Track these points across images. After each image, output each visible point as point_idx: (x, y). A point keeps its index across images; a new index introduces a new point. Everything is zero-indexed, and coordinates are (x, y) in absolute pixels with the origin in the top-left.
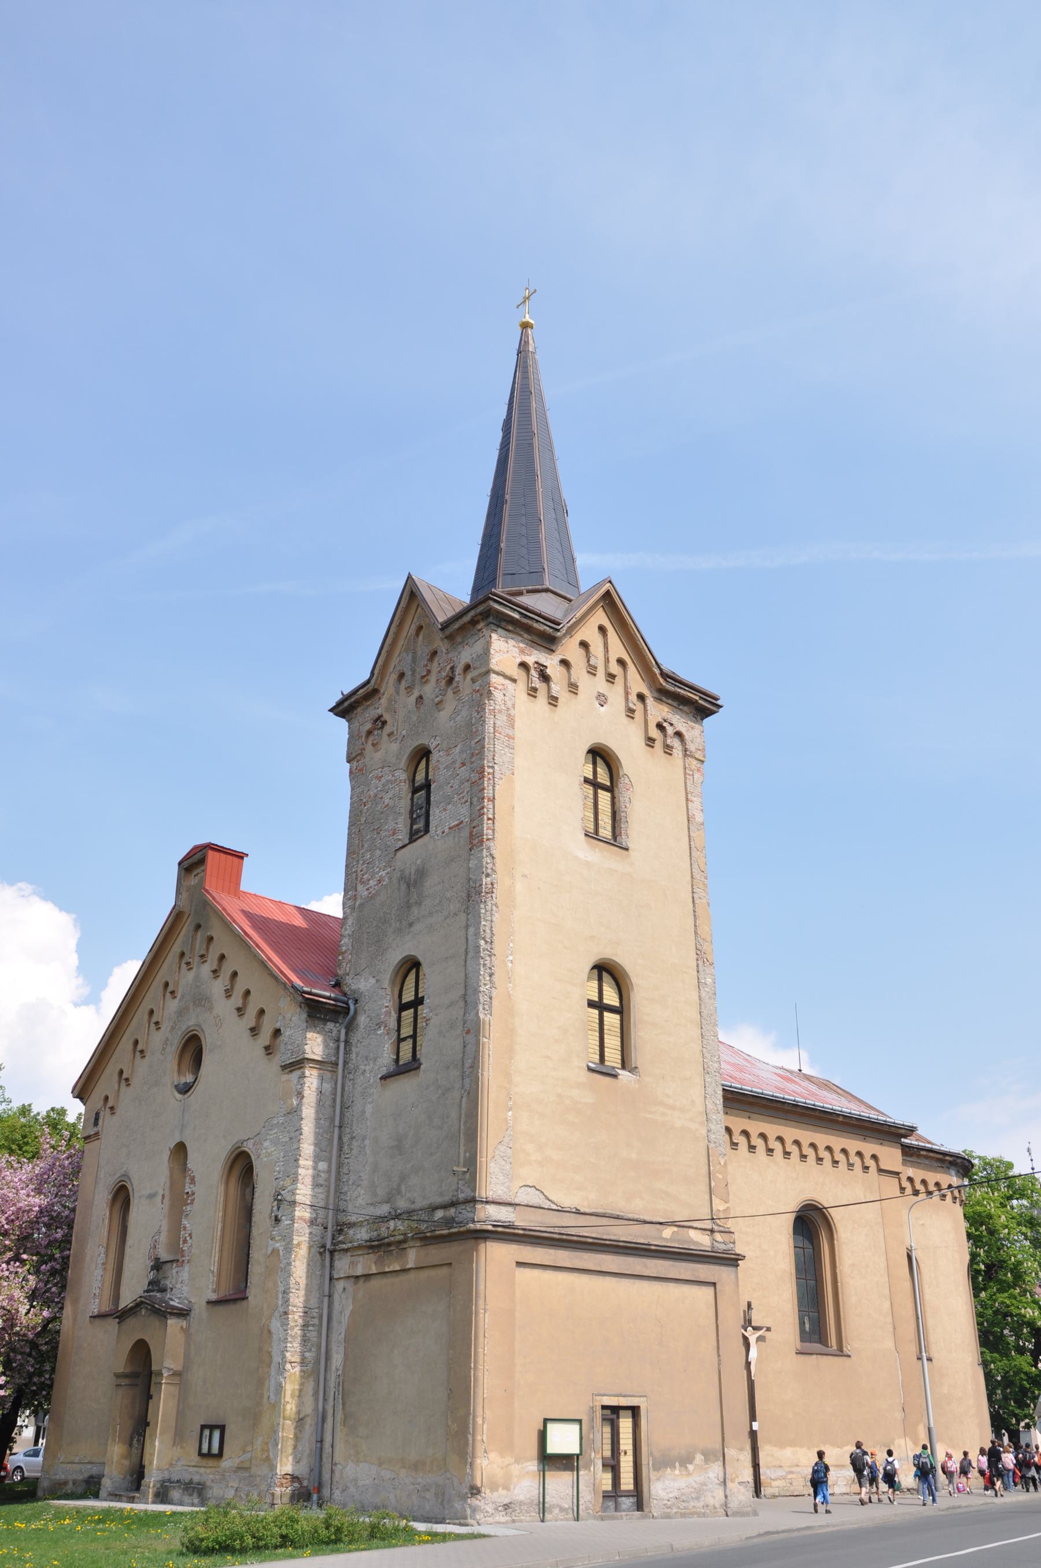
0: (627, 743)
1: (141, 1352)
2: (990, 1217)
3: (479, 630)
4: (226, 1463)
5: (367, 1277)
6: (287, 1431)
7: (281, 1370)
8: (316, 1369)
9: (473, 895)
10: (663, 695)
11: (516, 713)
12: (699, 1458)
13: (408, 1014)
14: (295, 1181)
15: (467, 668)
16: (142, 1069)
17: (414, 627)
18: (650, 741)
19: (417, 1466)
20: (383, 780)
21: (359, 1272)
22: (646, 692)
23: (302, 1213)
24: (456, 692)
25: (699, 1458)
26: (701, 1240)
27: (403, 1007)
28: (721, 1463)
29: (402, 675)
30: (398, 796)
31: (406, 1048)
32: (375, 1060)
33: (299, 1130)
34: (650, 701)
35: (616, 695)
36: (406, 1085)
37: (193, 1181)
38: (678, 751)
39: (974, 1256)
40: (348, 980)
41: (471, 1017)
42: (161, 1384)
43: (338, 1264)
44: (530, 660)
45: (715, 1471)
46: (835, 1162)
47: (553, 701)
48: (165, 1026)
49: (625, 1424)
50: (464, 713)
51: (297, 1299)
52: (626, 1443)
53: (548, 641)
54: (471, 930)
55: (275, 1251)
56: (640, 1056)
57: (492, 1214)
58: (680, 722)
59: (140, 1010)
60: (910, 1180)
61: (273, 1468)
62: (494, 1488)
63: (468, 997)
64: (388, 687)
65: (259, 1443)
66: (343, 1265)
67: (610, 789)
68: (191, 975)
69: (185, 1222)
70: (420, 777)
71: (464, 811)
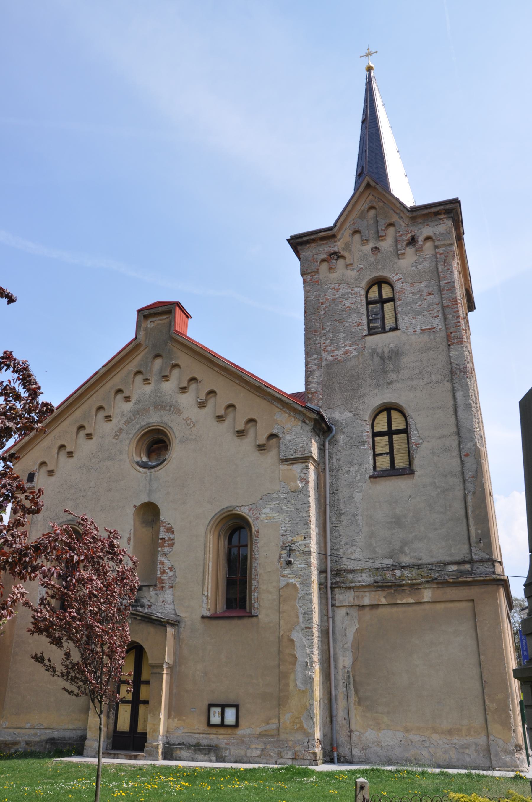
3: (440, 219)
4: (240, 732)
19: (450, 732)
20: (341, 291)
21: (367, 601)
32: (360, 465)
37: (170, 530)
42: (163, 674)
48: (117, 422)
64: (345, 236)
66: (345, 597)
68: (148, 389)
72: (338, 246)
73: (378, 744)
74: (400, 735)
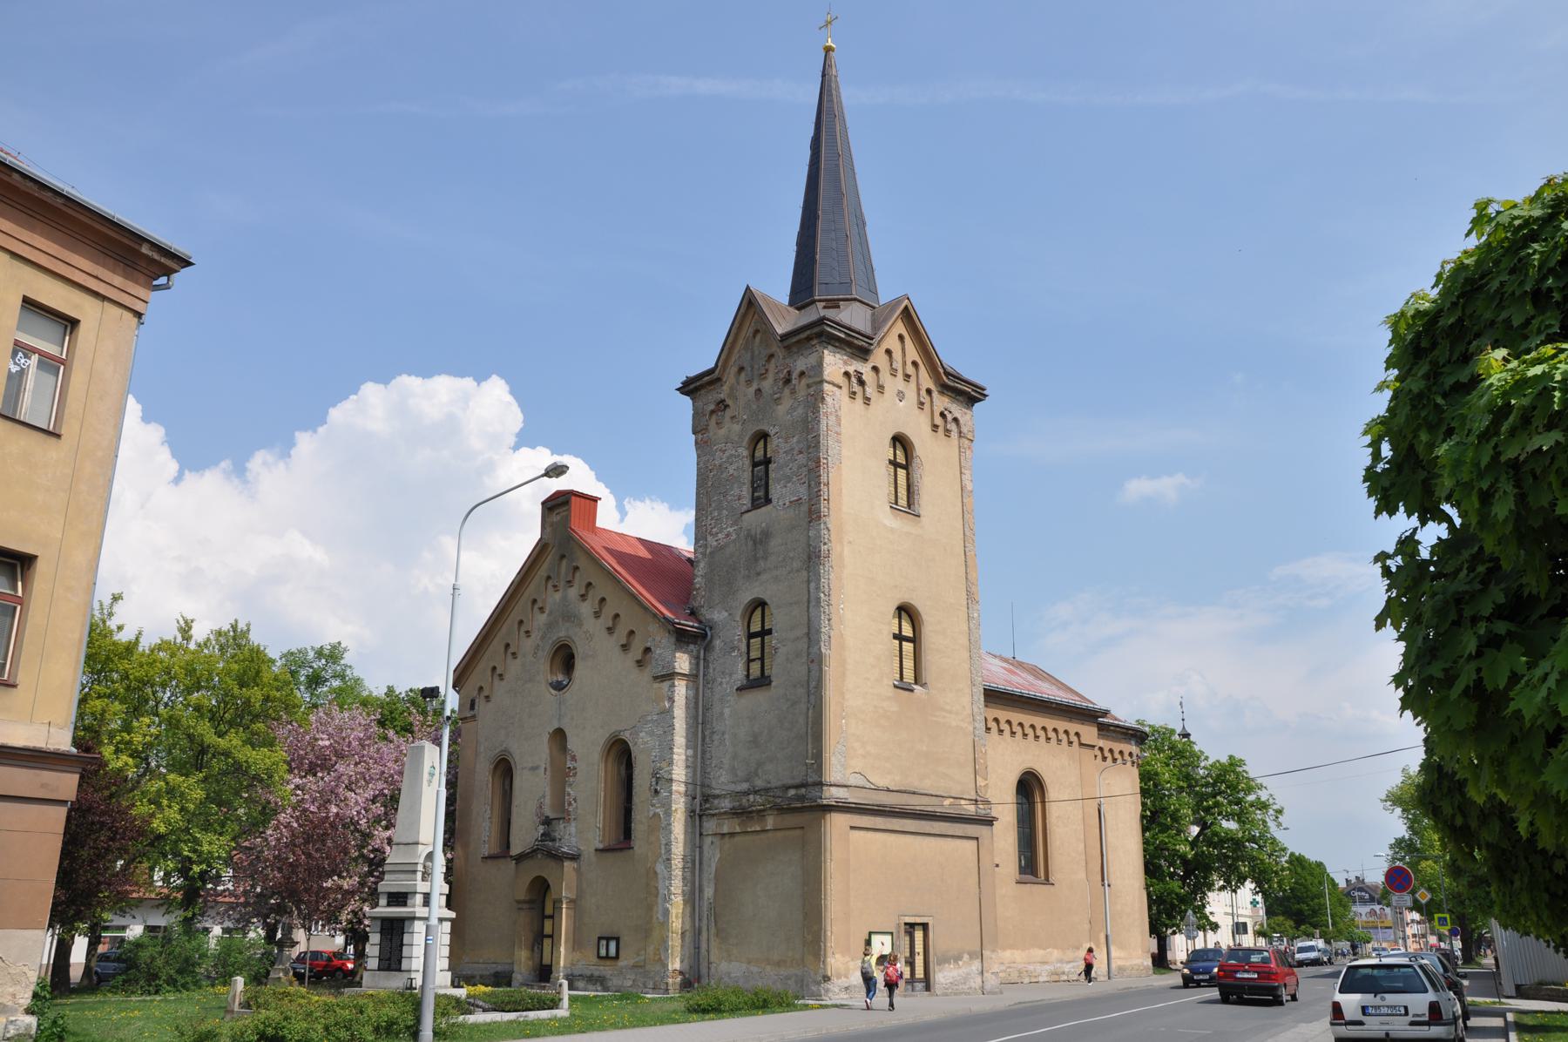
0: (918, 429)
1: (541, 888)
2: (1157, 774)
4: (622, 963)
5: (732, 834)
6: (675, 942)
7: (667, 899)
8: (693, 897)
9: (812, 558)
10: (945, 389)
11: (842, 413)
12: (966, 957)
13: (756, 642)
14: (671, 763)
15: (802, 374)
16: (513, 668)
17: (751, 330)
18: (935, 427)
19: (779, 964)
21: (725, 830)
22: (932, 387)
23: (679, 788)
24: (793, 392)
25: (966, 957)
26: (971, 809)
27: (751, 636)
28: (1114, 965)
29: (741, 369)
30: (740, 466)
31: (755, 667)
33: (672, 726)
34: (935, 394)
35: (910, 391)
36: (758, 697)
37: (574, 758)
38: (954, 434)
39: (1144, 804)
40: (703, 611)
41: (815, 650)
43: (705, 824)
44: (851, 369)
45: (976, 965)
46: (1048, 739)
47: (867, 401)
48: (535, 635)
49: (919, 935)
50: (800, 411)
51: (678, 849)
52: (919, 948)
53: (863, 353)
54: (812, 585)
55: (656, 815)
56: (929, 673)
57: (833, 794)
58: (957, 410)
59: (509, 621)
60: (1101, 749)
61: (665, 966)
62: (839, 977)
63: (811, 636)
64: (730, 377)
65: (651, 949)
66: (710, 826)
67: (906, 467)
68: (558, 596)
69: (568, 789)
70: (759, 454)
71: (803, 491)
72: (723, 392)
73: (729, 974)
74: (744, 966)
